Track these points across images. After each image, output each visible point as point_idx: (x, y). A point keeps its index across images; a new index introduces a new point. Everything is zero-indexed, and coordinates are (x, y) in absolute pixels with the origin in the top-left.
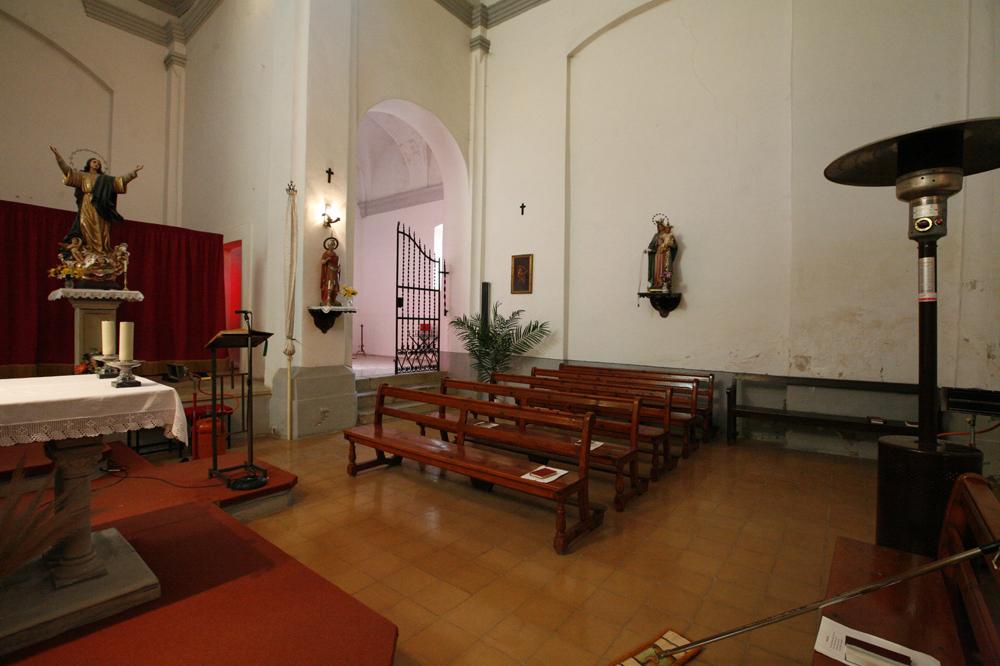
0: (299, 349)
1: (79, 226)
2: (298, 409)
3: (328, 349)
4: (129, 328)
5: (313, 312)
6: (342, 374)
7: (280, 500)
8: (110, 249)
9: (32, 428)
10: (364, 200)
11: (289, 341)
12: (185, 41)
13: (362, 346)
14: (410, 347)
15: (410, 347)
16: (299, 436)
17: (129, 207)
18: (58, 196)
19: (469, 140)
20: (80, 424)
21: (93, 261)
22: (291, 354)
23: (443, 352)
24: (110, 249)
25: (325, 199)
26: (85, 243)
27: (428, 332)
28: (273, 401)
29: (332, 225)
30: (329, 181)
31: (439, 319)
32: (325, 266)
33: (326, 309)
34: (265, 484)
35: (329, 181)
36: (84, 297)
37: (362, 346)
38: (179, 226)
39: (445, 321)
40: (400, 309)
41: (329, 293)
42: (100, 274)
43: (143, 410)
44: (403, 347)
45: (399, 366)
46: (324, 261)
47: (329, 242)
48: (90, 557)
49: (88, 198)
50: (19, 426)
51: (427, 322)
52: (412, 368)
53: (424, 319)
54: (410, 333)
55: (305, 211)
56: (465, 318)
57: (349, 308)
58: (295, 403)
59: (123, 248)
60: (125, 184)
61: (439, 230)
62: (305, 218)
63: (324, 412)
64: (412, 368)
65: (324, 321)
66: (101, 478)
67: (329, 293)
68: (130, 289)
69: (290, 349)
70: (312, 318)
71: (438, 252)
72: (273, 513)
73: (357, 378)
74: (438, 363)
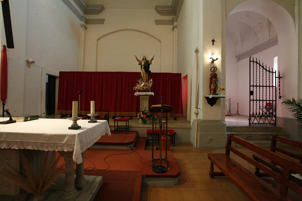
0: (201, 112)
1: (141, 76)
2: (200, 137)
3: (214, 113)
4: (93, 103)
5: (207, 98)
6: (219, 124)
7: (171, 182)
8: (148, 81)
9: (29, 143)
10: (238, 55)
11: (196, 109)
12: (177, 21)
13: (238, 111)
14: (258, 114)
15: (258, 114)
16: (199, 147)
17: (153, 69)
18: (137, 69)
19: (294, 5)
20: (42, 144)
21: (143, 84)
22: (197, 114)
23: (277, 117)
24: (148, 81)
25: (211, 52)
26: (142, 80)
27: (271, 107)
28: (192, 131)
29: (214, 62)
30: (213, 44)
31: (276, 101)
32: (211, 79)
33: (211, 97)
34: (165, 172)
35: (213, 44)
36: (140, 95)
37: (238, 111)
38: (176, 73)
39: (279, 102)
40: (252, 96)
41: (214, 91)
42: (145, 88)
43: (64, 142)
44: (253, 113)
45: (251, 122)
46: (211, 77)
47: (213, 69)
48: (71, 193)
49: (143, 67)
50: (25, 142)
51: (271, 102)
52: (259, 123)
53: (270, 101)
54: (259, 108)
55: (203, 58)
56: (294, 100)
57: (221, 95)
58: (198, 133)
59: (151, 80)
60: (151, 62)
61: (276, 59)
62: (203, 61)
63: (211, 139)
64: (259, 123)
65: (212, 102)
66: (129, 150)
67: (214, 91)
68: (151, 92)
69: (196, 112)
70: (207, 100)
71: (276, 68)
72: (166, 187)
73: (227, 126)
74: (275, 122)
